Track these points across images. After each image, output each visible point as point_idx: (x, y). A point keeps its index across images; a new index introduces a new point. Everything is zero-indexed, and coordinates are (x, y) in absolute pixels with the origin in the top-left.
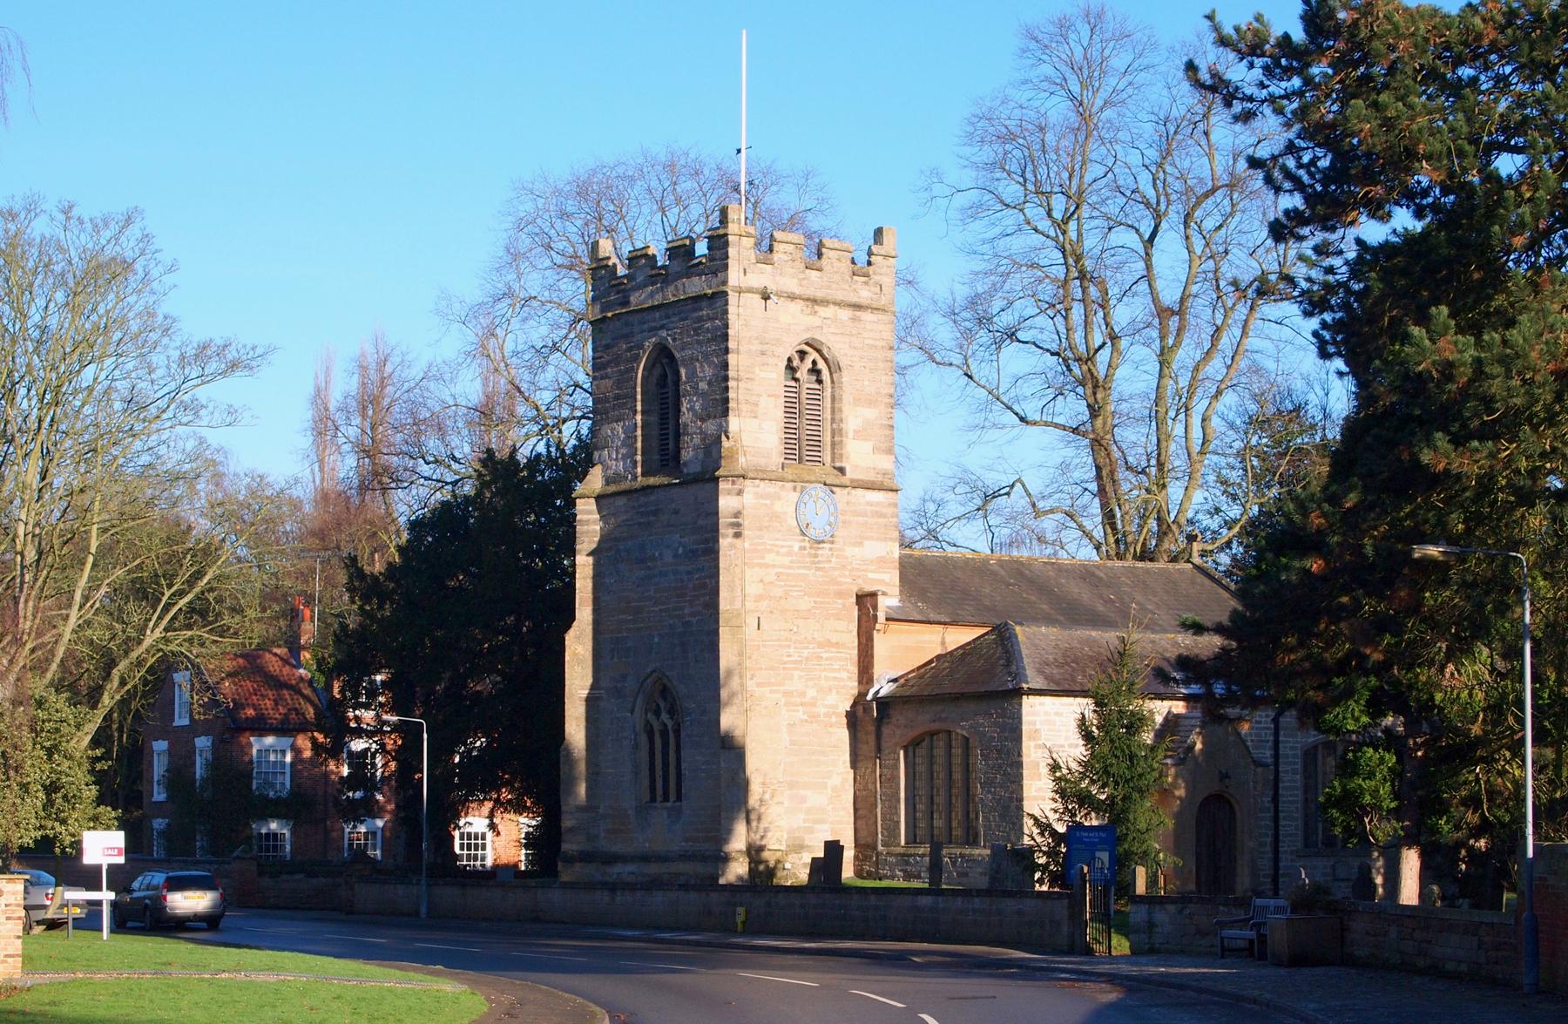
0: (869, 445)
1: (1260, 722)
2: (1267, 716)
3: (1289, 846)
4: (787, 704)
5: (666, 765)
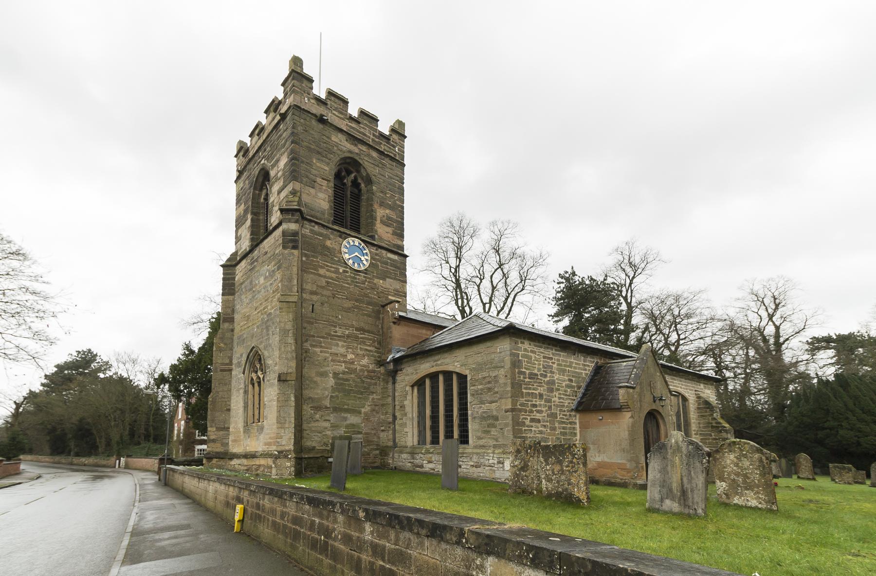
0: (390, 230)
4: (333, 360)
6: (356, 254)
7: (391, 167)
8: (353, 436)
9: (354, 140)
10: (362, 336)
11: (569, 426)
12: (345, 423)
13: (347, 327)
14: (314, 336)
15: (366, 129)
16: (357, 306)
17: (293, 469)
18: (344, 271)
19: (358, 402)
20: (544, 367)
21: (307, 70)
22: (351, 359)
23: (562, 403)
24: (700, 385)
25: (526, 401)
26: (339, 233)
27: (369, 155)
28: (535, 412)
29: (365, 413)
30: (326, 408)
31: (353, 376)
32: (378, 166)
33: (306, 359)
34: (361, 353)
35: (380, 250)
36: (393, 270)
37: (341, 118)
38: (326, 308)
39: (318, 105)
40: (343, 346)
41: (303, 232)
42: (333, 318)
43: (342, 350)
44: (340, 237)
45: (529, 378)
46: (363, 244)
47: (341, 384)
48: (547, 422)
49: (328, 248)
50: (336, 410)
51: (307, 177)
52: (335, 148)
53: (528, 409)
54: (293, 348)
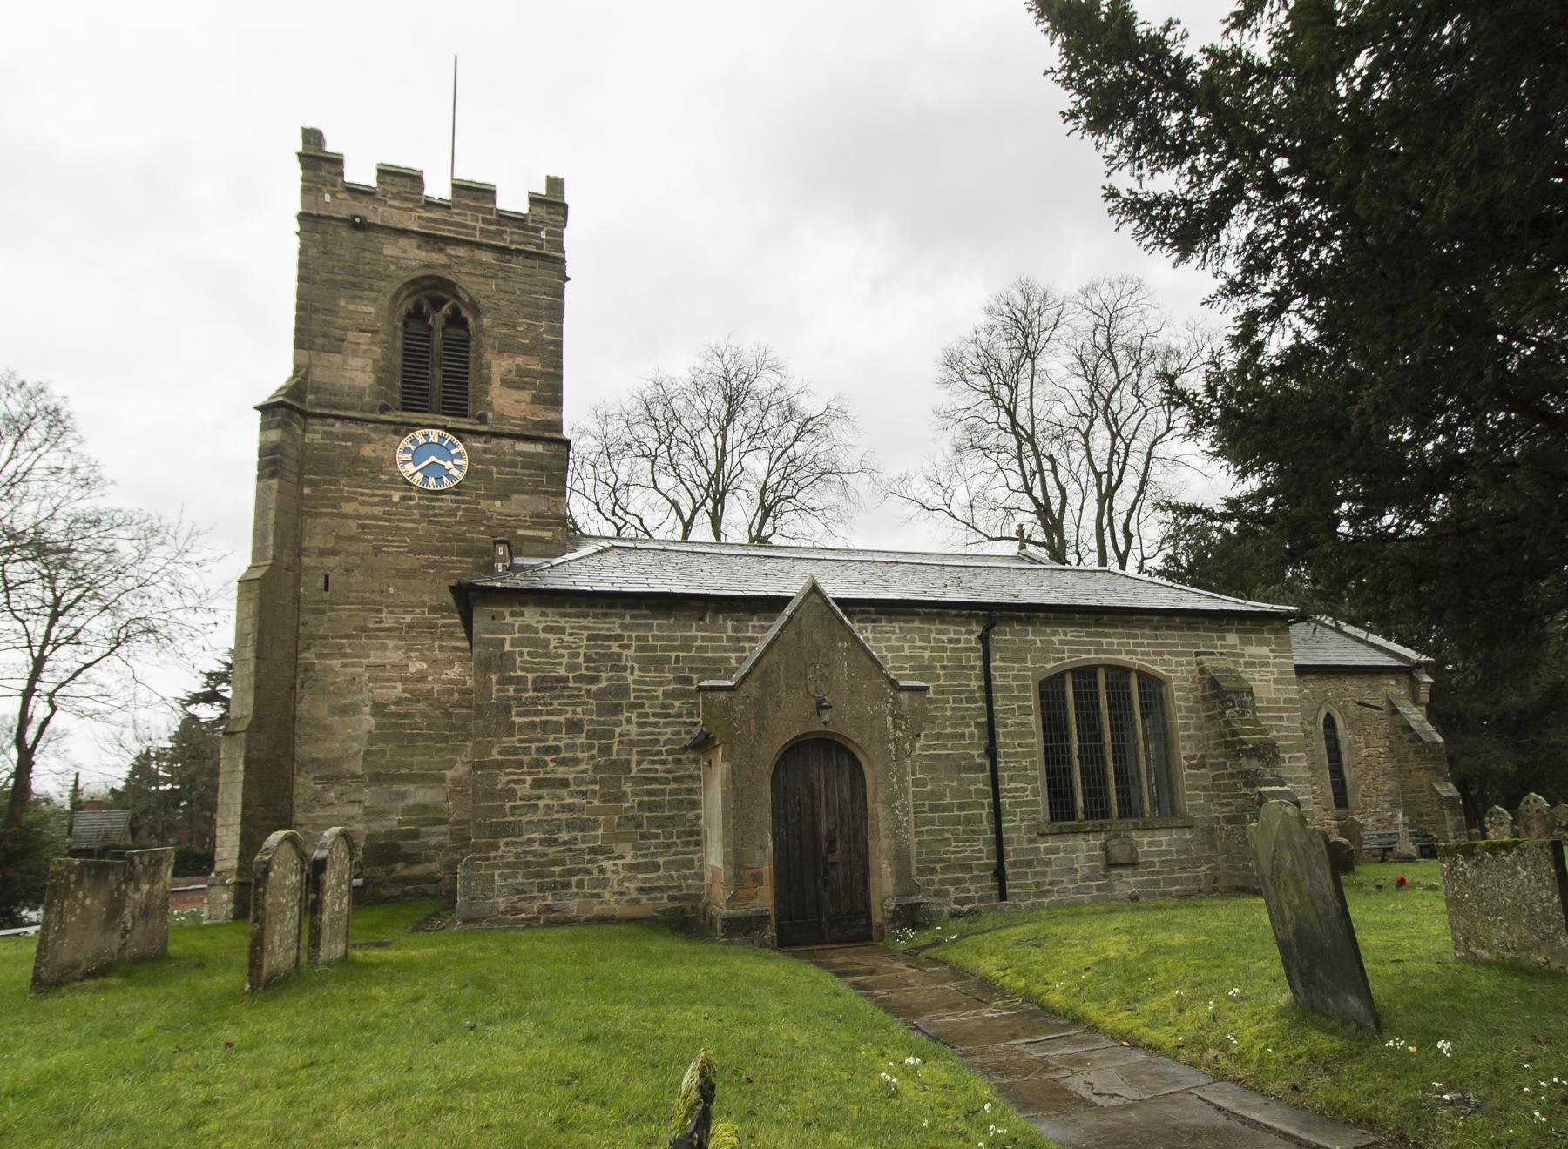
0: (526, 395)
1: (959, 641)
2: (970, 632)
3: (1022, 820)
5: (1092, 755)
6: (433, 459)
7: (529, 271)
8: (422, 829)
9: (436, 243)
10: (444, 621)
11: (673, 785)
12: (402, 805)
13: (406, 607)
14: (326, 637)
15: (466, 215)
16: (435, 561)
17: (231, 906)
18: (403, 499)
19: (436, 758)
20: (588, 659)
21: (331, 147)
22: (418, 671)
23: (652, 734)
24: (1224, 639)
25: (521, 741)
26: (392, 427)
27: (472, 261)
28: (551, 765)
29: (453, 780)
30: (355, 776)
31: (422, 706)
32: (495, 277)
33: (307, 684)
34: (443, 655)
35: (495, 441)
36: (530, 475)
37: (405, 209)
38: (356, 577)
39: (355, 199)
40: (396, 648)
41: (307, 441)
42: (373, 596)
43: (395, 657)
44: (396, 432)
45: (535, 690)
46: (450, 437)
47: (393, 726)
48: (594, 782)
49: (365, 461)
50: (376, 779)
51: (325, 335)
52: (393, 267)
53: (526, 759)
54: (252, 667)
